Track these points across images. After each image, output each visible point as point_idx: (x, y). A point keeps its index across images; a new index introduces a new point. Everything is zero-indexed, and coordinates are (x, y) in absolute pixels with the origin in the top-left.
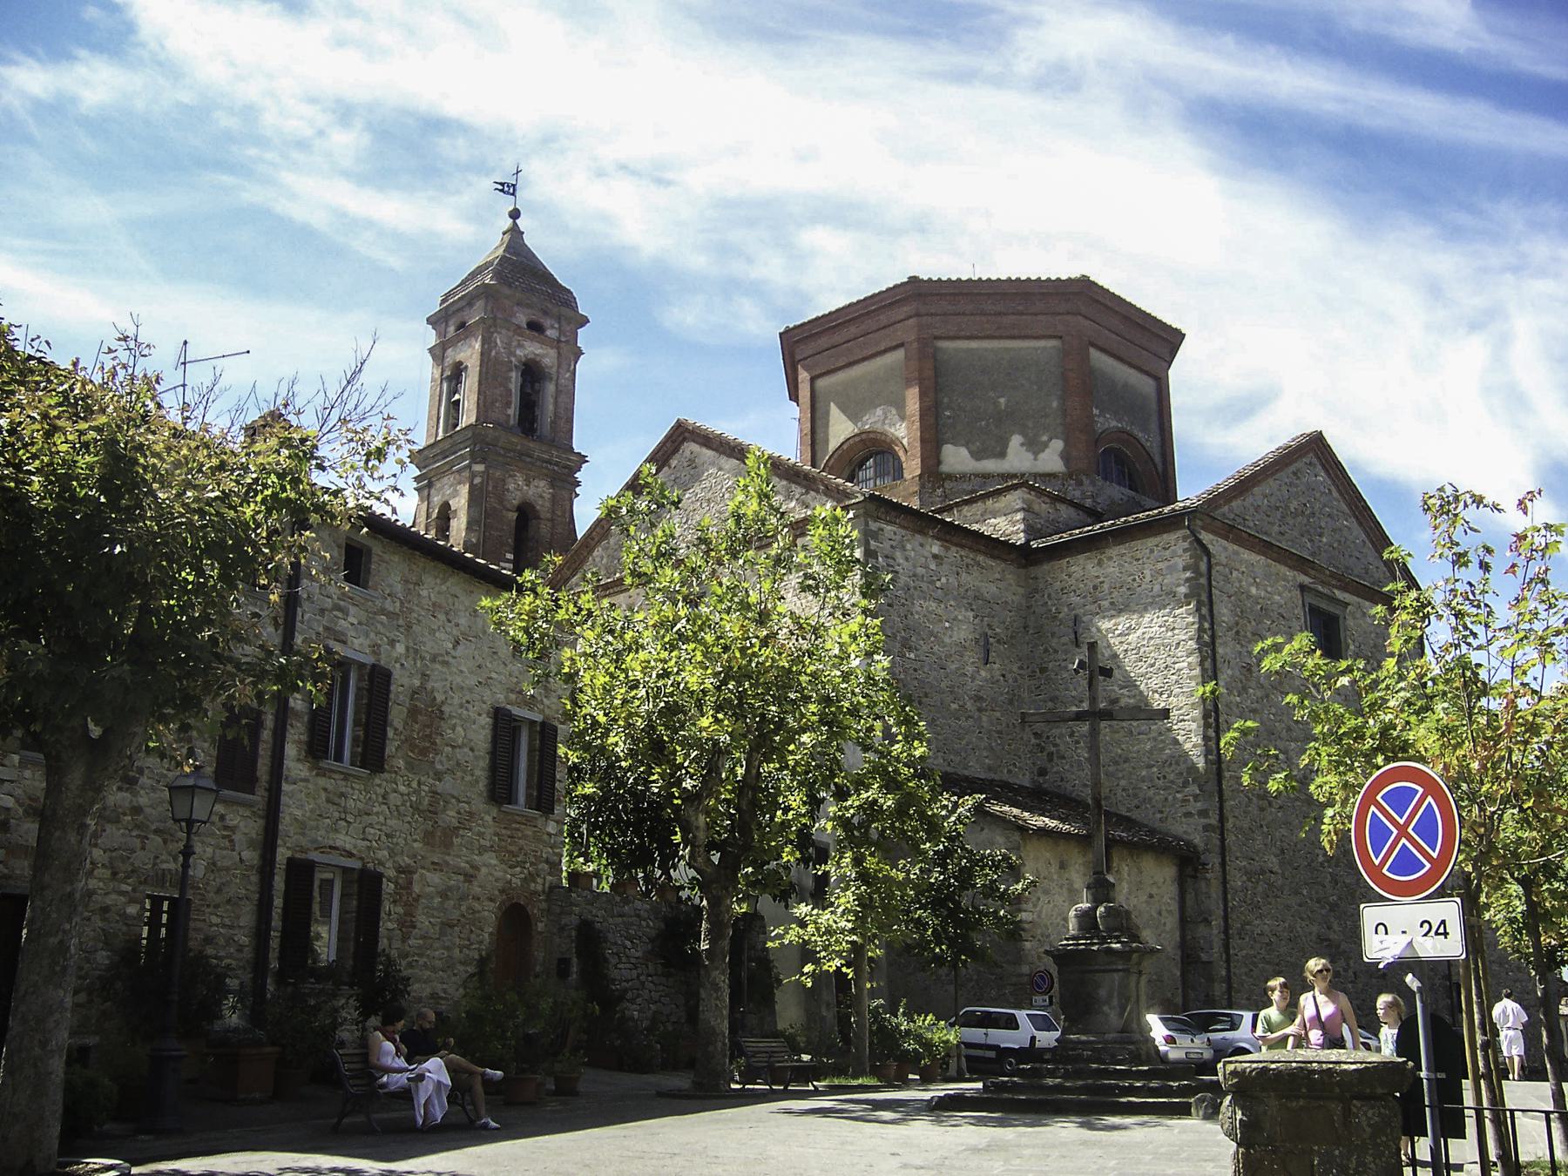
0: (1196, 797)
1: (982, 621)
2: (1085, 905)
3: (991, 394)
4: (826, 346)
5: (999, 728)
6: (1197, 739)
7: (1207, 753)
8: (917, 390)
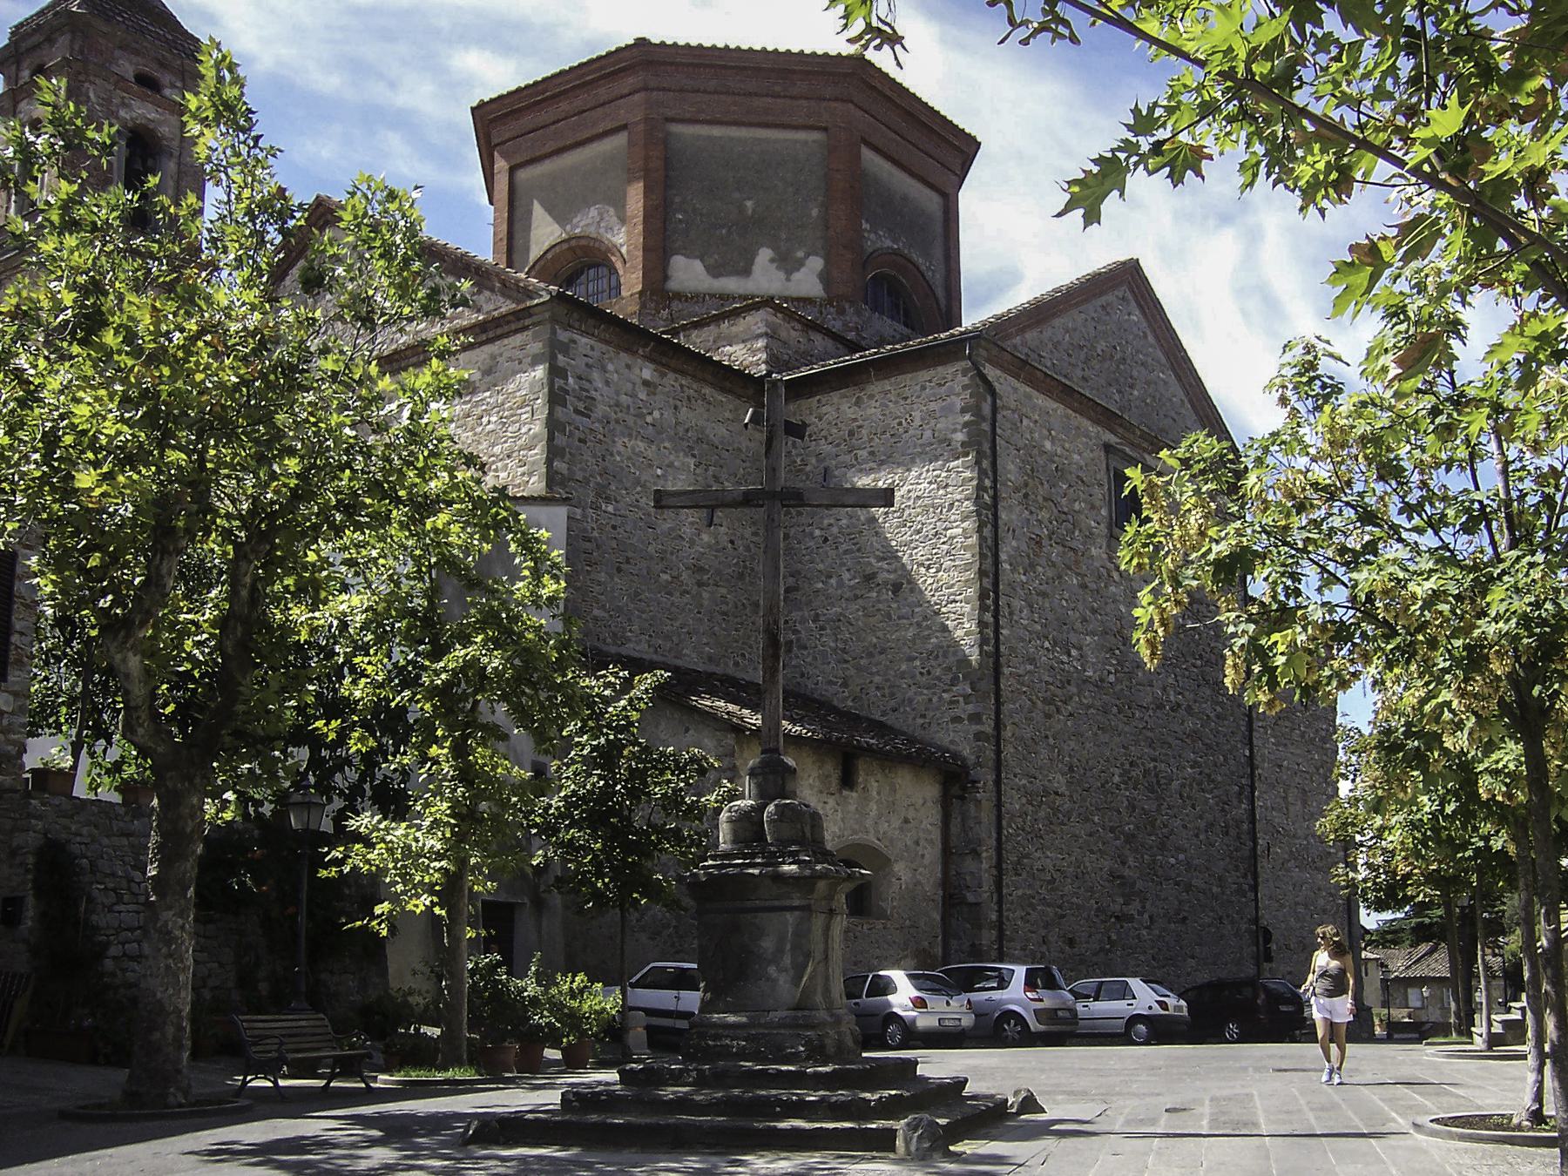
0: (967, 698)
1: (706, 470)
2: (746, 803)
3: (737, 195)
4: (531, 126)
5: (724, 608)
6: (969, 625)
7: (983, 642)
8: (641, 184)
